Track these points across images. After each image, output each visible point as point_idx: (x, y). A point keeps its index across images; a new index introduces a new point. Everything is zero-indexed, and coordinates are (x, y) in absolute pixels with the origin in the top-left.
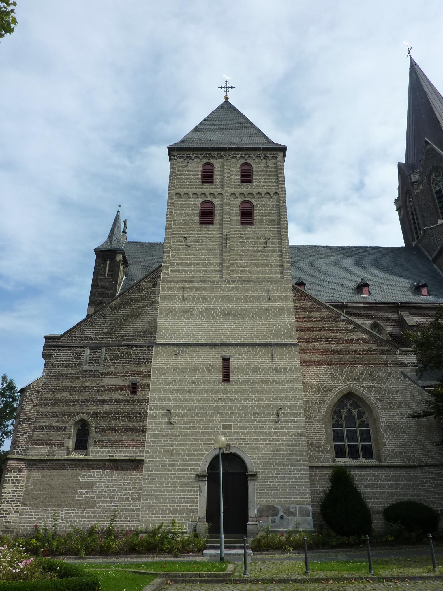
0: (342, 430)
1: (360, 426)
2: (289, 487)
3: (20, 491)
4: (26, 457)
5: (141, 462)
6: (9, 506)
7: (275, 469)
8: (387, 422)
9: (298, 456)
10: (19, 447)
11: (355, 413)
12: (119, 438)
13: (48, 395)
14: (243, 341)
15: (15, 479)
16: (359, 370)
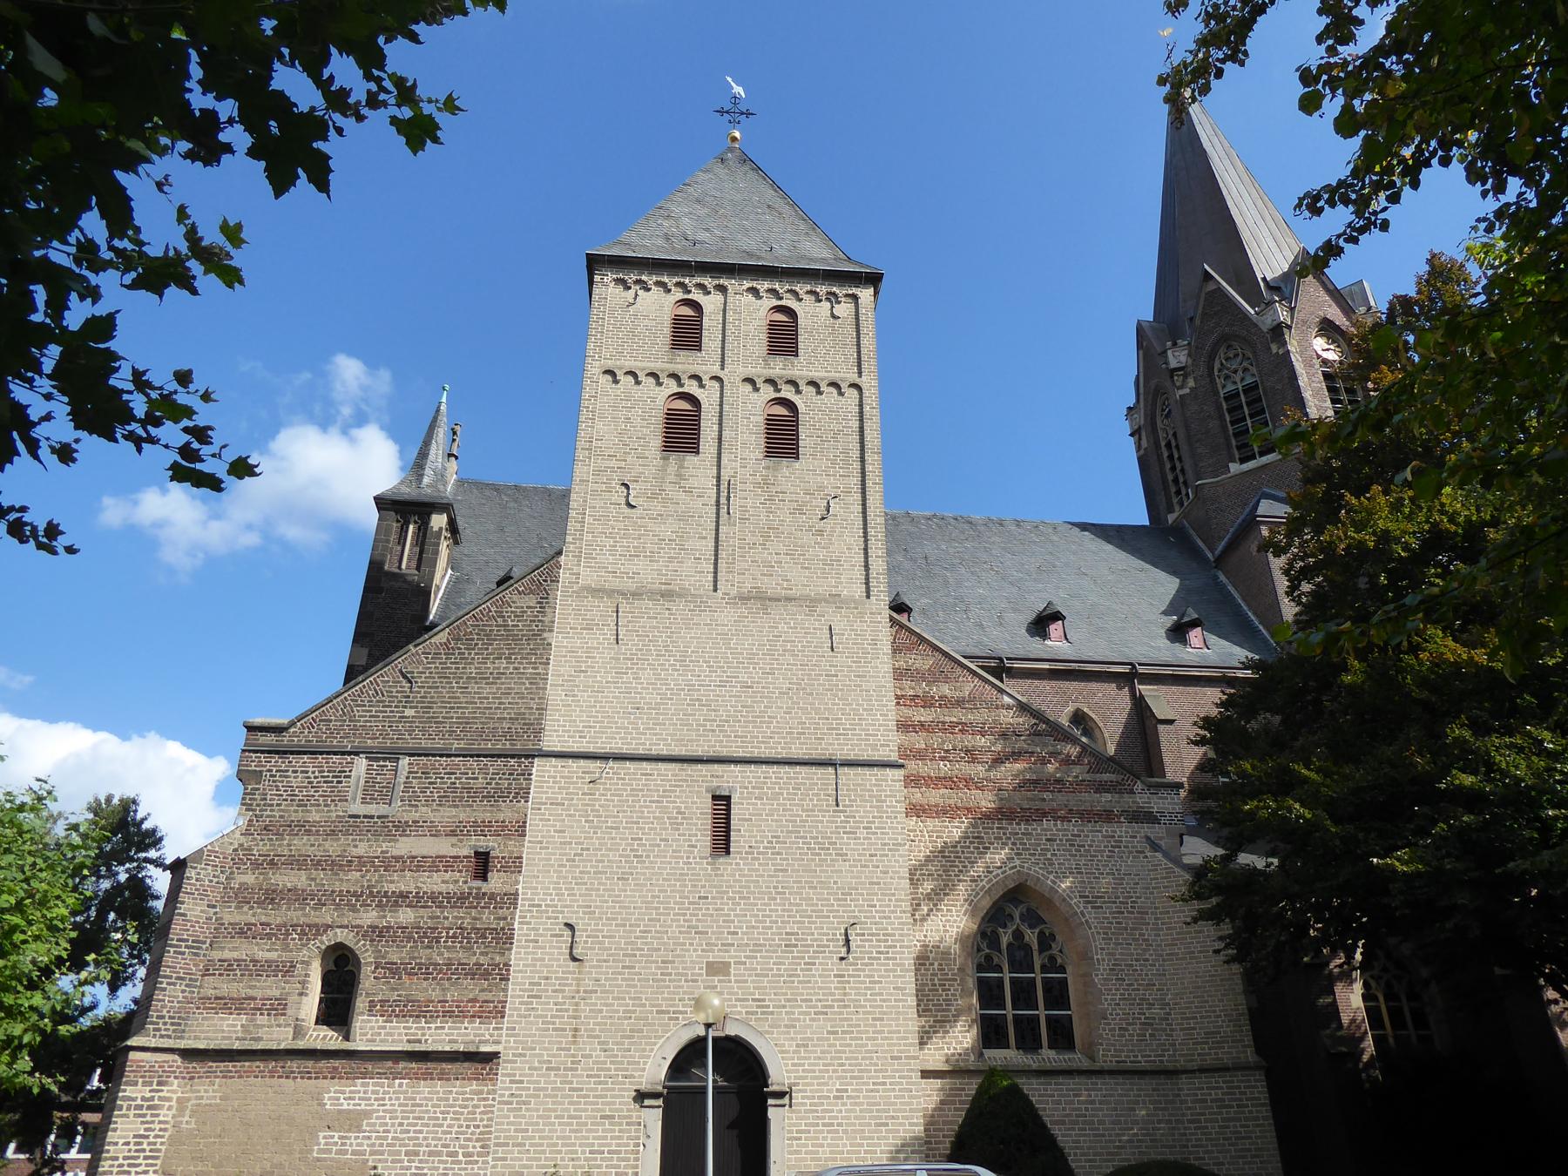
3: (156, 1136)
4: (182, 1044)
5: (490, 1058)
11: (1031, 936)
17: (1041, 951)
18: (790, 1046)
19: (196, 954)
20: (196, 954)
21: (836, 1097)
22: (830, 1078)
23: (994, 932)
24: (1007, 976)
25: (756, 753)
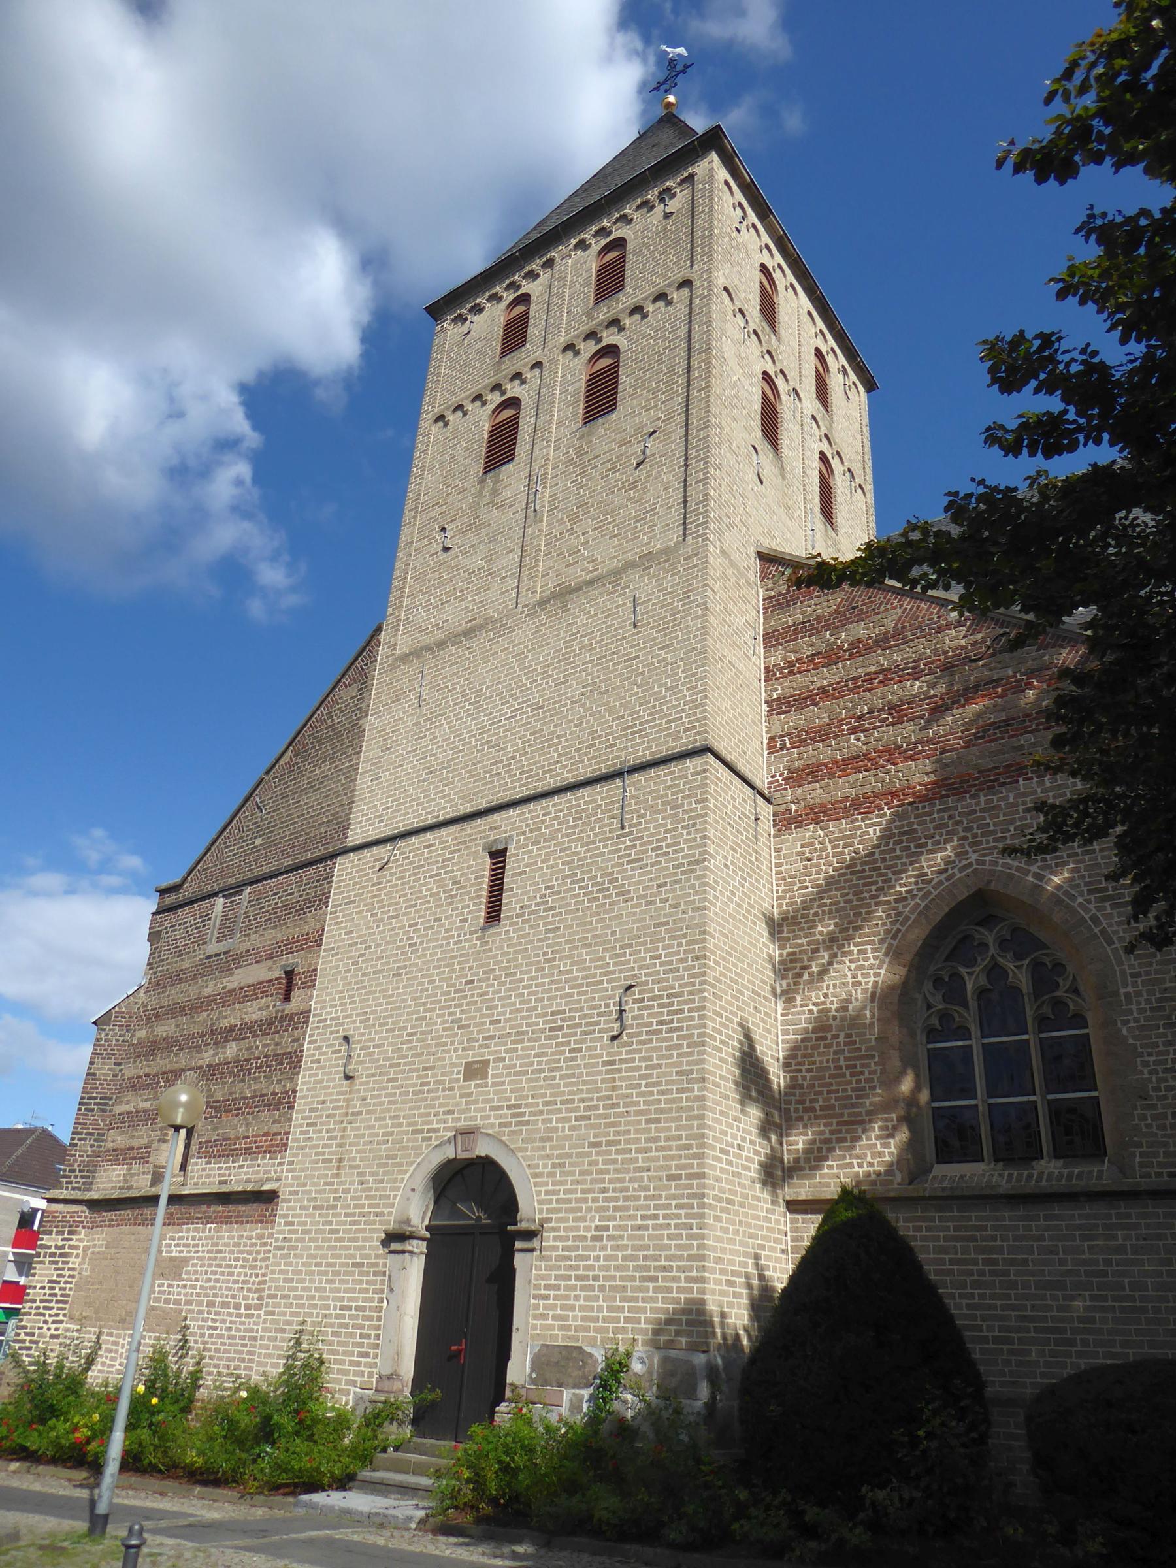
0: (967, 1051)
1: (1043, 1023)
2: (633, 1279)
3: (66, 1282)
4: (88, 1195)
5: (268, 1198)
6: (39, 1321)
7: (598, 1210)
8: (1149, 993)
9: (672, 1158)
10: (74, 1171)
11: (1020, 976)
12: (241, 1131)
13: (141, 1034)
14: (551, 783)
15: (58, 1252)
16: (1024, 795)
17: (1037, 994)
18: (544, 1167)
19: (104, 1111)
20: (104, 1111)
21: (594, 1238)
22: (589, 1210)
23: (956, 976)
24: (975, 1043)
25: (540, 787)
